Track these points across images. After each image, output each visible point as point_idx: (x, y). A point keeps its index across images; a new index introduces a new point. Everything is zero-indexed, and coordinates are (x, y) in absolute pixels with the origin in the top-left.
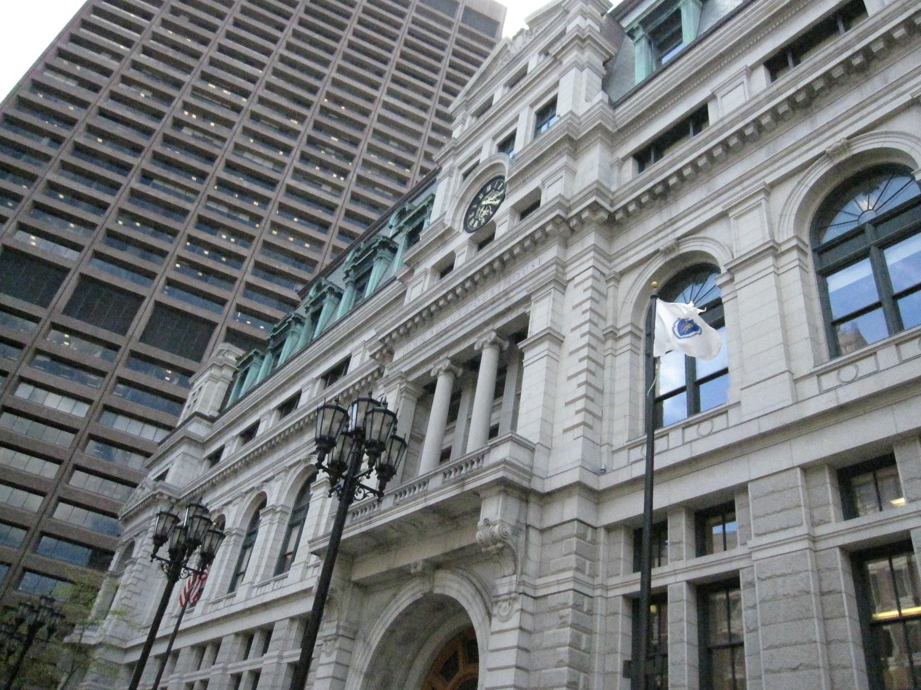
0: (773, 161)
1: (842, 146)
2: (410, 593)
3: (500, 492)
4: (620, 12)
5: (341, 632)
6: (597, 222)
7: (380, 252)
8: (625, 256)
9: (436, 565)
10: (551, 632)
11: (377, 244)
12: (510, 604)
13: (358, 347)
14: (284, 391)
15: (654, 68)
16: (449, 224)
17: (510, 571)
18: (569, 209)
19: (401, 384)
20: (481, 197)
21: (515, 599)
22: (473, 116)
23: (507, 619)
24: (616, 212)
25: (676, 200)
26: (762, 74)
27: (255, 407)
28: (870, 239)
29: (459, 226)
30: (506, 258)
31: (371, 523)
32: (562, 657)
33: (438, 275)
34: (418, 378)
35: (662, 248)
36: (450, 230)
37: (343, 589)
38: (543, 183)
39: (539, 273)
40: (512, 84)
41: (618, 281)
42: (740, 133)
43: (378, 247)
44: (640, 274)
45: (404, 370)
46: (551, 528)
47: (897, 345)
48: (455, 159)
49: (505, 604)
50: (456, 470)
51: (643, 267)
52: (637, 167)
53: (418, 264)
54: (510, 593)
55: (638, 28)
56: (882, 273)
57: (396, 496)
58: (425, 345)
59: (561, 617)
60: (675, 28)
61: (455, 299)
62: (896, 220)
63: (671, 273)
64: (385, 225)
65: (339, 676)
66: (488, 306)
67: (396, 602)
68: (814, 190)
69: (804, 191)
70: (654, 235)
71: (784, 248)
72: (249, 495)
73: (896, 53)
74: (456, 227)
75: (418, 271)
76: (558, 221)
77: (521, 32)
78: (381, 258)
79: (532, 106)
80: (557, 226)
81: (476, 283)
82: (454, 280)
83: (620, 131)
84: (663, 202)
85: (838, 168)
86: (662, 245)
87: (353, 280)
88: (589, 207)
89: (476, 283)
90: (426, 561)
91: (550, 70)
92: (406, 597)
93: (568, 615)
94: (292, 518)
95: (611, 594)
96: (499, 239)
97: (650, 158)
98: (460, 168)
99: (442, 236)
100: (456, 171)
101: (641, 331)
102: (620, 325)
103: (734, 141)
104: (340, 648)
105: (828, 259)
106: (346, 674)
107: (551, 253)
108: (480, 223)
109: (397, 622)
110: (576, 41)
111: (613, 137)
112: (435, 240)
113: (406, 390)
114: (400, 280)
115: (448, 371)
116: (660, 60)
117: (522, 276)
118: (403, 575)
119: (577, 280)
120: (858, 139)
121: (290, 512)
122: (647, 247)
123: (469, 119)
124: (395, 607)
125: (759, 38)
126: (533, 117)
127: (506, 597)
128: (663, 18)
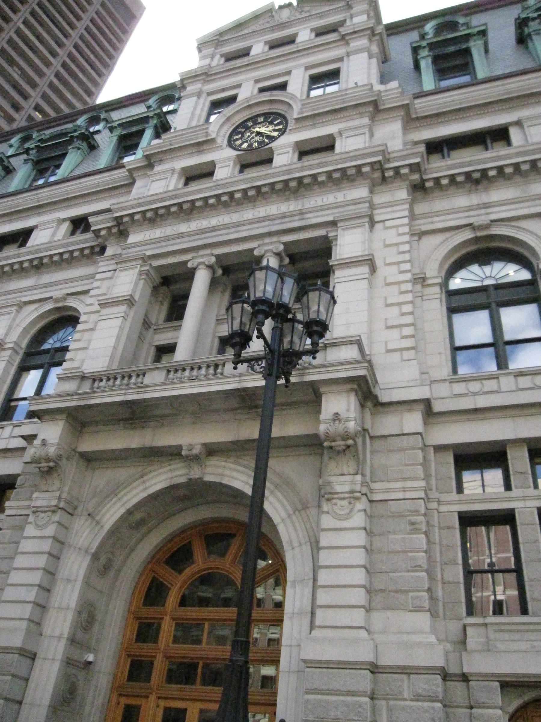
0: (36, 287)
1: (487, 225)
2: (170, 475)
3: (352, 390)
4: (67, 118)
5: (62, 505)
6: (411, 181)
7: (78, 143)
8: (430, 220)
9: (212, 451)
10: (398, 537)
11: (76, 134)
12: (350, 503)
13: (49, 222)
14: (10, 221)
15: (114, 163)
16: (213, 136)
17: (352, 471)
18: (388, 161)
19: (141, 266)
20: (261, 119)
21: (357, 499)
22: (222, 56)
23: (348, 516)
24: (428, 180)
25: (486, 189)
26: (66, 227)
27: (39, 209)
28: (494, 296)
29: (222, 141)
30: (306, 181)
31: (144, 392)
32: (420, 563)
33: (238, 168)
34: (162, 266)
35: (476, 224)
36: (213, 140)
37: (68, 459)
38: (340, 133)
39: (347, 205)
40: (274, 45)
41: (420, 238)
42: (517, 166)
43: (77, 137)
44: (447, 239)
45: (148, 253)
46: (385, 437)
47: (515, 376)
48: (203, 85)
49: (345, 503)
50: (138, 376)
51: (453, 233)
52: (71, 229)
53: (161, 161)
54: (352, 492)
55: (424, 47)
56: (496, 325)
57: (169, 371)
58: (181, 235)
59: (412, 524)
60: (134, 142)
61: (187, 210)
62: (468, 296)
63: (473, 248)
64: (6, 141)
65: (55, 553)
66: (232, 227)
67: (144, 482)
68: (42, 316)
69: (35, 315)
70: (464, 211)
71: (430, 282)
72: (33, 307)
73: (501, 182)
74: (219, 140)
75: (158, 168)
76: (377, 166)
77: (290, 5)
78: (79, 149)
79: (257, 81)
80: (373, 170)
81: (228, 201)
82: (200, 190)
83: (417, 119)
84: (474, 188)
85: (476, 240)
86: (476, 221)
87: (35, 160)
88: (410, 165)
89: (228, 201)
90: (204, 445)
91: (333, 45)
92: (160, 479)
93: (421, 522)
94: (23, 360)
95: (443, 508)
96: (217, 180)
97: (80, 228)
98: (209, 94)
99: (199, 144)
100: (204, 95)
101: (21, 348)
102: (7, 341)
103: (445, 182)
104: (59, 523)
105: (459, 303)
106: (61, 551)
107: (360, 192)
108: (250, 145)
109: (138, 506)
110: (369, 32)
111: (411, 120)
112: (191, 145)
113: (148, 273)
114: (129, 170)
115: (210, 267)
116: (121, 158)
117: (320, 203)
118: (174, 454)
119: (388, 224)
120: (500, 225)
121: (22, 352)
122: (458, 218)
123: (218, 57)
124: (142, 487)
125: (497, 109)
126: (208, 104)
127: (347, 495)
128: (135, 129)
